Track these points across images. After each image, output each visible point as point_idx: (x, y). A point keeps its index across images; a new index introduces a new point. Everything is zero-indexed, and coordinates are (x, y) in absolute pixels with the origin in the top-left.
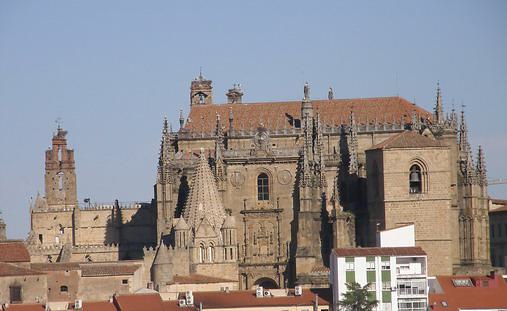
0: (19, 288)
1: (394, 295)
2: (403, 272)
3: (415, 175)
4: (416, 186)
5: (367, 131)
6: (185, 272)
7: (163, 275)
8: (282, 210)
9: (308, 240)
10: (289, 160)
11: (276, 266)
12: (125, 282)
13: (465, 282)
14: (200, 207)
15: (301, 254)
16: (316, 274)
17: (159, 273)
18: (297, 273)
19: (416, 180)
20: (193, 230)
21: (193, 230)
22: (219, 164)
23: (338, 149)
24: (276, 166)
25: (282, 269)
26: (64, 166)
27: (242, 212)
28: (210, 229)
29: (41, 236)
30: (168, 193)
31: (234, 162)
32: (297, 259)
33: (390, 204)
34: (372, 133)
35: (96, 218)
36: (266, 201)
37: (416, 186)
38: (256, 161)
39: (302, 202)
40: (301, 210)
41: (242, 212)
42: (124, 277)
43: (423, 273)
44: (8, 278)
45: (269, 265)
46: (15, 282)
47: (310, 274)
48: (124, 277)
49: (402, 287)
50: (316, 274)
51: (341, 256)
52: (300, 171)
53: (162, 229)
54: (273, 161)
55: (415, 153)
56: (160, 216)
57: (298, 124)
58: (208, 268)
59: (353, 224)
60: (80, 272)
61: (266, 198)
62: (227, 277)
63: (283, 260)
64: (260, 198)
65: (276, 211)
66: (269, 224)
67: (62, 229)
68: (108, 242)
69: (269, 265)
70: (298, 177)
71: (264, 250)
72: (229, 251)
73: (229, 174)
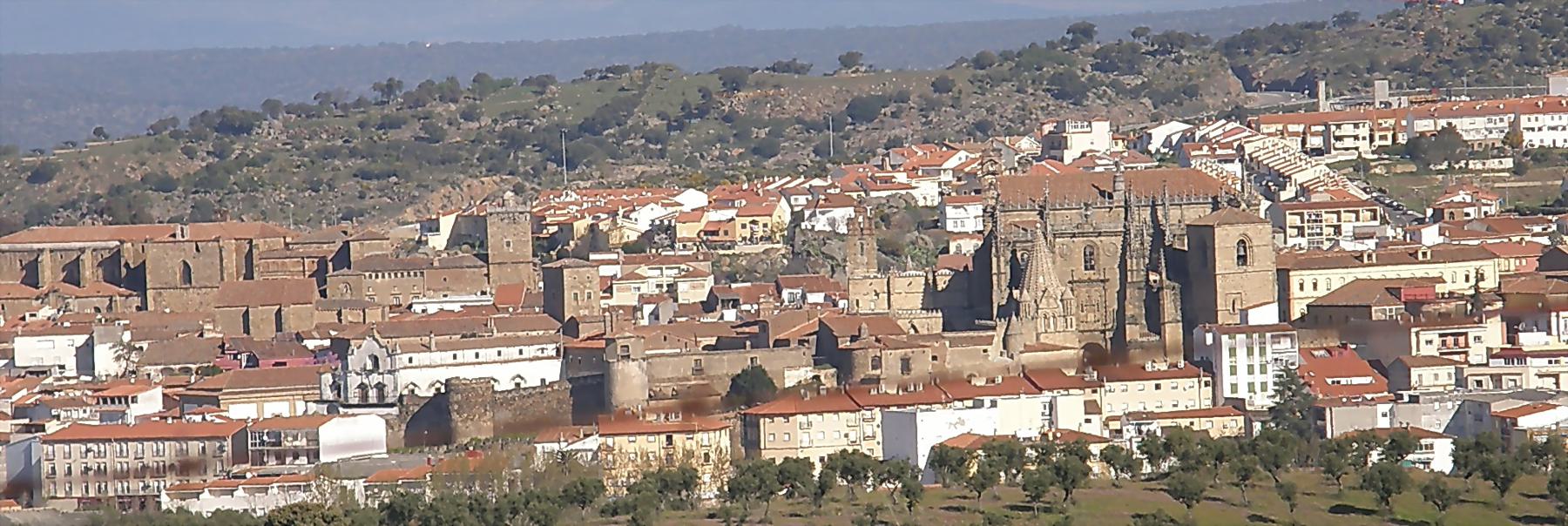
0: (908, 359)
1: (1269, 367)
2: (1276, 346)
3: (1242, 249)
4: (1242, 259)
5: (1176, 202)
6: (1032, 341)
7: (1016, 344)
8: (1108, 280)
9: (1134, 308)
10: (1116, 234)
11: (1103, 332)
12: (985, 351)
13: (1322, 352)
14: (1041, 279)
15: (1131, 320)
16: (1145, 339)
17: (1012, 341)
18: (1128, 339)
19: (1242, 253)
20: (1036, 301)
21: (1036, 301)
22: (1050, 237)
23: (1149, 219)
24: (1102, 238)
25: (1109, 335)
26: (865, 232)
27: (1070, 282)
28: (1051, 300)
29: (857, 301)
30: (1002, 265)
31: (1062, 235)
32: (1127, 326)
33: (1296, 301)
34: (1181, 205)
35: (910, 284)
36: (1092, 272)
37: (1242, 259)
38: (1083, 235)
39: (1129, 273)
40: (1129, 280)
41: (1070, 282)
42: (985, 347)
43: (1292, 348)
44: (900, 351)
45: (1095, 330)
46: (906, 354)
47: (1140, 340)
48: (985, 347)
49: (1276, 360)
50: (1145, 339)
51: (1225, 334)
52: (1126, 245)
53: (999, 297)
54: (1100, 234)
55: (1242, 228)
56: (995, 287)
57: (1111, 196)
58: (1051, 336)
59: (1178, 292)
60: (947, 343)
61: (1092, 268)
62: (1068, 345)
63: (1110, 326)
64: (1086, 269)
65: (1102, 281)
66: (1096, 293)
67: (877, 294)
68: (926, 307)
69: (1095, 330)
70: (1124, 249)
71: (1091, 317)
72: (1069, 321)
73: (1057, 247)
